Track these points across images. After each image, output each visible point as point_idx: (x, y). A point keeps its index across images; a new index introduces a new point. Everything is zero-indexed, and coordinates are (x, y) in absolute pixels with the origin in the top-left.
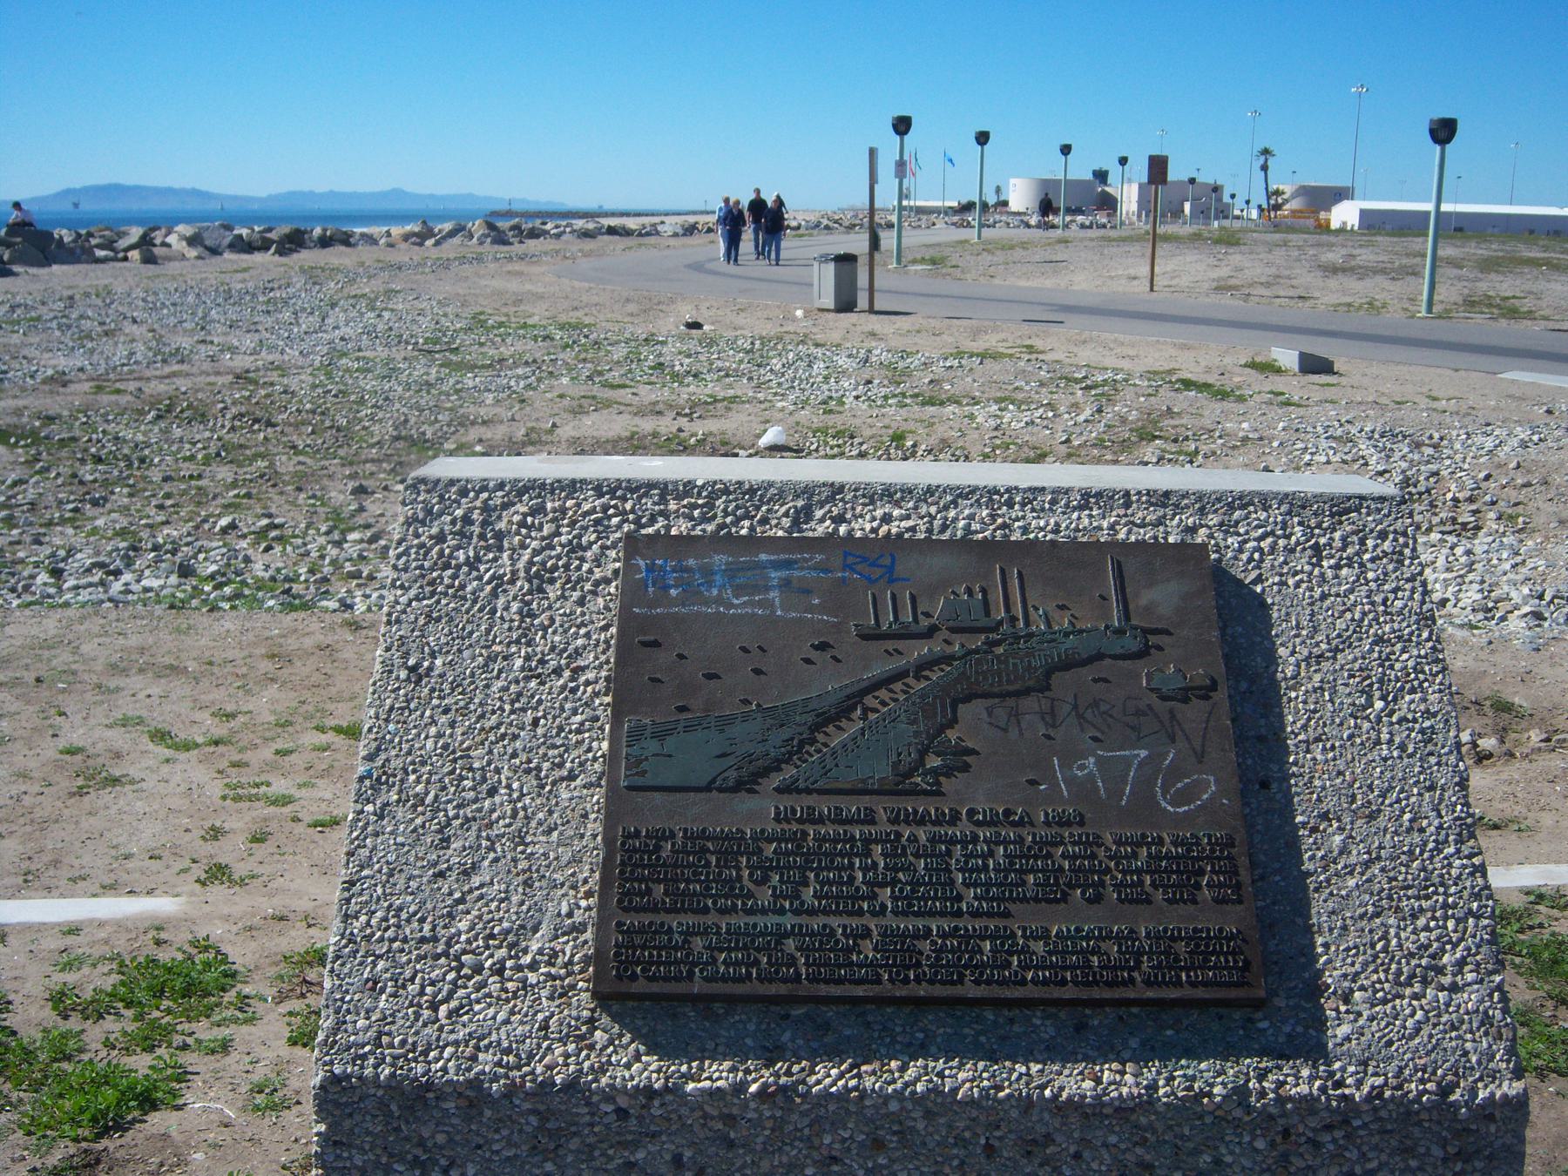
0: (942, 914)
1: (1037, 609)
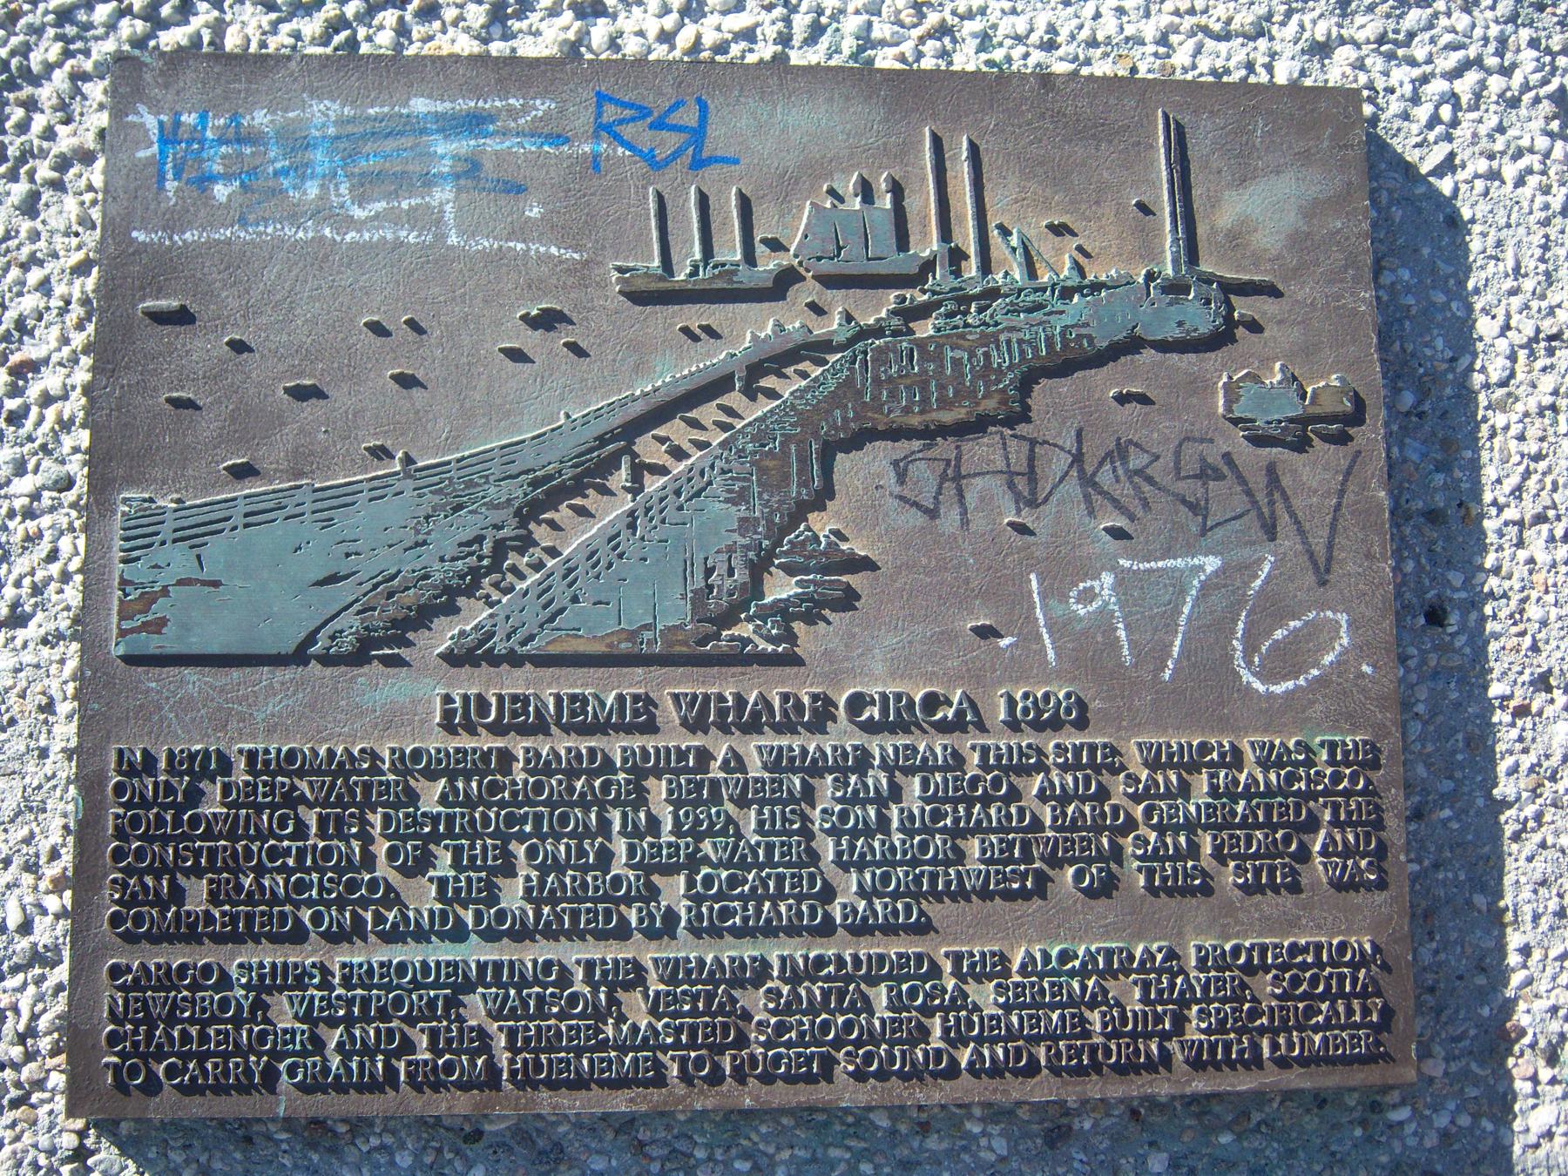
0: (793, 931)
1: (1005, 232)
